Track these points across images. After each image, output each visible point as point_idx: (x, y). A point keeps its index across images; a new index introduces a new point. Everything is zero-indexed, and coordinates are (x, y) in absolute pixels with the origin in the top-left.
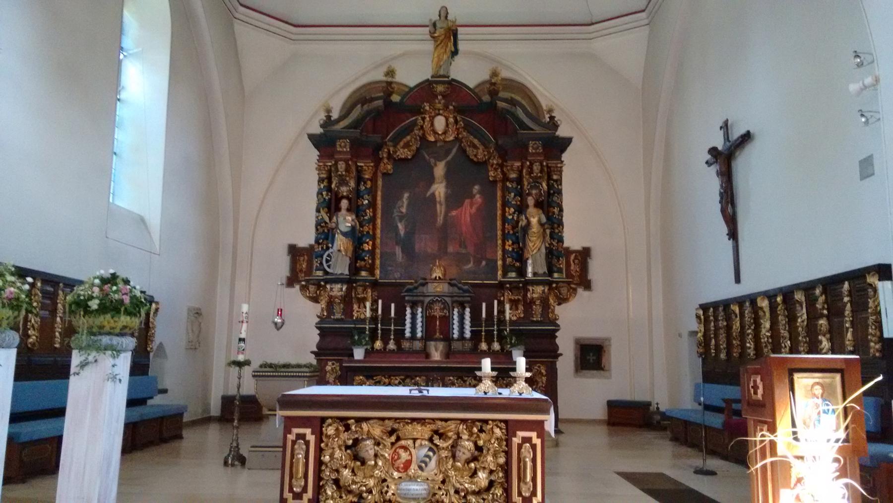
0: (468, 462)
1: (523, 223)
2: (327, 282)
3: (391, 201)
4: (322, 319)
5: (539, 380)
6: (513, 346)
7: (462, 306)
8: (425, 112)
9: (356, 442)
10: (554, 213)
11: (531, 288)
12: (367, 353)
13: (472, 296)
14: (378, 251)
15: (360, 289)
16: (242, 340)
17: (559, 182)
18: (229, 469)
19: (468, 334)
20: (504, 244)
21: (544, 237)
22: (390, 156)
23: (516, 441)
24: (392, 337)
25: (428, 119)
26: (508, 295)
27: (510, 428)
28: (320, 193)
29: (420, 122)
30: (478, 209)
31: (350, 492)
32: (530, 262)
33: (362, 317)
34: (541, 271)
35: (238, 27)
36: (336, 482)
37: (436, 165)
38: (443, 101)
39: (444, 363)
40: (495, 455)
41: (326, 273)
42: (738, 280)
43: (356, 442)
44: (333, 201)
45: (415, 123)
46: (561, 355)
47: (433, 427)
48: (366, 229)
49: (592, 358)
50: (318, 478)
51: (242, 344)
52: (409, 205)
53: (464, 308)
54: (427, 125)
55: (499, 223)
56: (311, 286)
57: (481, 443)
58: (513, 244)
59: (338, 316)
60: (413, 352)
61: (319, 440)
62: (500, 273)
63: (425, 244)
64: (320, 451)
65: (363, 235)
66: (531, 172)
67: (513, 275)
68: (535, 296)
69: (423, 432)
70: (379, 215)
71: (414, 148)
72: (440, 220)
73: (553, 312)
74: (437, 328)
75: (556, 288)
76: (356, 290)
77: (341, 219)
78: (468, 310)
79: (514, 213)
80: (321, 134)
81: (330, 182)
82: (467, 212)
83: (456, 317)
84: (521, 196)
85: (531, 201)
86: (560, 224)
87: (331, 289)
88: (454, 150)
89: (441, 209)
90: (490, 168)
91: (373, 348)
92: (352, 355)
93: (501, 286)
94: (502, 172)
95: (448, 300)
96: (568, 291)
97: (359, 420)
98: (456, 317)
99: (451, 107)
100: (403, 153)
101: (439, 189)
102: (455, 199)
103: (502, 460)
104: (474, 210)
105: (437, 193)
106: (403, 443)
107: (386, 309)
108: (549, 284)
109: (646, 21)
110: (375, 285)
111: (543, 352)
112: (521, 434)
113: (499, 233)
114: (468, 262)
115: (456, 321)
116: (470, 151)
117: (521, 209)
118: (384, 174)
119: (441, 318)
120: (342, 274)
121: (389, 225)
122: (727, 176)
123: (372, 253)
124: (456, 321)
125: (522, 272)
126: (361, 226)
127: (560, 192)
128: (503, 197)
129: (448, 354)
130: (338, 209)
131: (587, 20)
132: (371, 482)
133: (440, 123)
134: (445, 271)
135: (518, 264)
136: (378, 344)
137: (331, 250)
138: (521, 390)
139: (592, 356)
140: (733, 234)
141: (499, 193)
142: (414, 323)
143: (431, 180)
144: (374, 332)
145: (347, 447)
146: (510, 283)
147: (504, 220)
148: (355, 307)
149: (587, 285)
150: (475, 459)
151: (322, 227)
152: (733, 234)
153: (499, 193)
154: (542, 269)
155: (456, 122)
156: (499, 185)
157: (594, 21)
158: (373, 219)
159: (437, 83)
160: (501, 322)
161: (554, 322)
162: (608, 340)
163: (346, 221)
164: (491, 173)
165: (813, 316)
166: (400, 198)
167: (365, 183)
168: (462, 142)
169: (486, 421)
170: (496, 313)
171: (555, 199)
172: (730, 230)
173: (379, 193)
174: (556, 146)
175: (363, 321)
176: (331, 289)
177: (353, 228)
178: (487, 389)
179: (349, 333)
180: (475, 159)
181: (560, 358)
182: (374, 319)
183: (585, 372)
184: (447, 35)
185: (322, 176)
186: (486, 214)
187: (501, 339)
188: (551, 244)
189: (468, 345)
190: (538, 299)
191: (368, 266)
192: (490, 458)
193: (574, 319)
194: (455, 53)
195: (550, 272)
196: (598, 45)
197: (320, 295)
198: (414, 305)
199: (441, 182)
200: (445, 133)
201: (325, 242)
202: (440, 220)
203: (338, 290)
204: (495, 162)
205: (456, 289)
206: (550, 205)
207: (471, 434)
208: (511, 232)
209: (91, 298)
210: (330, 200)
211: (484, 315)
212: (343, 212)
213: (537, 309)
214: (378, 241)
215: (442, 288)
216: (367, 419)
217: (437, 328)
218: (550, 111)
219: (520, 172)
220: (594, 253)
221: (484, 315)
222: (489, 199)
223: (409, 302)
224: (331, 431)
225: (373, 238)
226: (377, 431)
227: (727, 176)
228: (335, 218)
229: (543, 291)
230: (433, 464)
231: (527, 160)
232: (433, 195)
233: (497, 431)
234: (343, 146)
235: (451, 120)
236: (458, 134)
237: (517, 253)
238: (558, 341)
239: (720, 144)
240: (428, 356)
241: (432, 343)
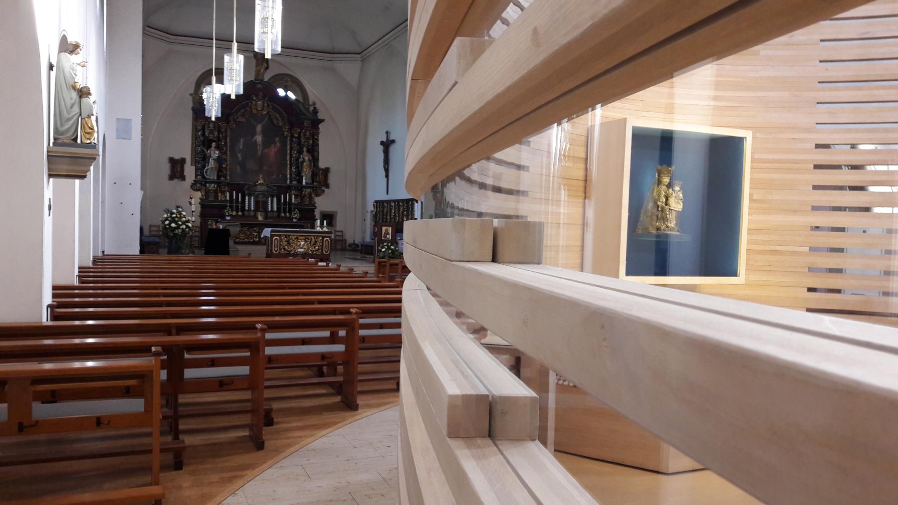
7: (272, 197)
17: (317, 140)
19: (275, 209)
20: (291, 168)
27: (323, 237)
60: (249, 217)
63: (251, 165)
66: (305, 135)
72: (260, 153)
74: (261, 206)
82: (273, 151)
85: (305, 149)
86: (318, 160)
89: (260, 148)
101: (259, 138)
102: (267, 144)
108: (313, 188)
110: (229, 184)
117: (300, 152)
125: (300, 181)
127: (318, 145)
129: (266, 218)
138: (325, 229)
139: (329, 218)
140: (387, 176)
152: (387, 176)
155: (268, 105)
165: (404, 210)
174: (316, 123)
178: (319, 229)
189: (276, 214)
195: (313, 182)
196: (336, 64)
198: (250, 195)
202: (260, 153)
206: (314, 151)
212: (213, 148)
215: (264, 188)
218: (314, 104)
219: (300, 134)
222: (284, 145)
239: (385, 140)
240: (257, 218)
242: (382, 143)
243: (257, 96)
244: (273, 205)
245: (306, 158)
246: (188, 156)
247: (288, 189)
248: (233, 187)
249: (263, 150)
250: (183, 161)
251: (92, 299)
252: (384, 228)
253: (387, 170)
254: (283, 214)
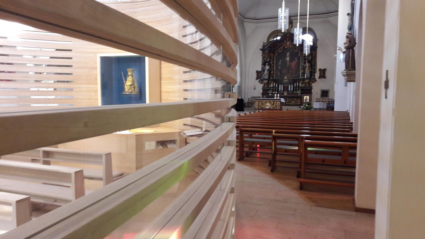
7: (291, 84)
19: (292, 90)
35: (245, 23)
63: (284, 71)
72: (288, 65)
82: (294, 64)
85: (307, 61)
89: (288, 63)
101: (288, 59)
102: (291, 61)
117: (305, 63)
125: (304, 76)
129: (288, 94)
138: (278, 98)
162: (329, 90)
178: (275, 98)
198: (281, 84)
202: (288, 65)
215: (287, 81)
243: (286, 40)
244: (291, 88)
245: (307, 65)
247: (299, 81)
248: (275, 81)
249: (290, 63)
251: (353, 138)
252: (305, 97)
254: (295, 92)
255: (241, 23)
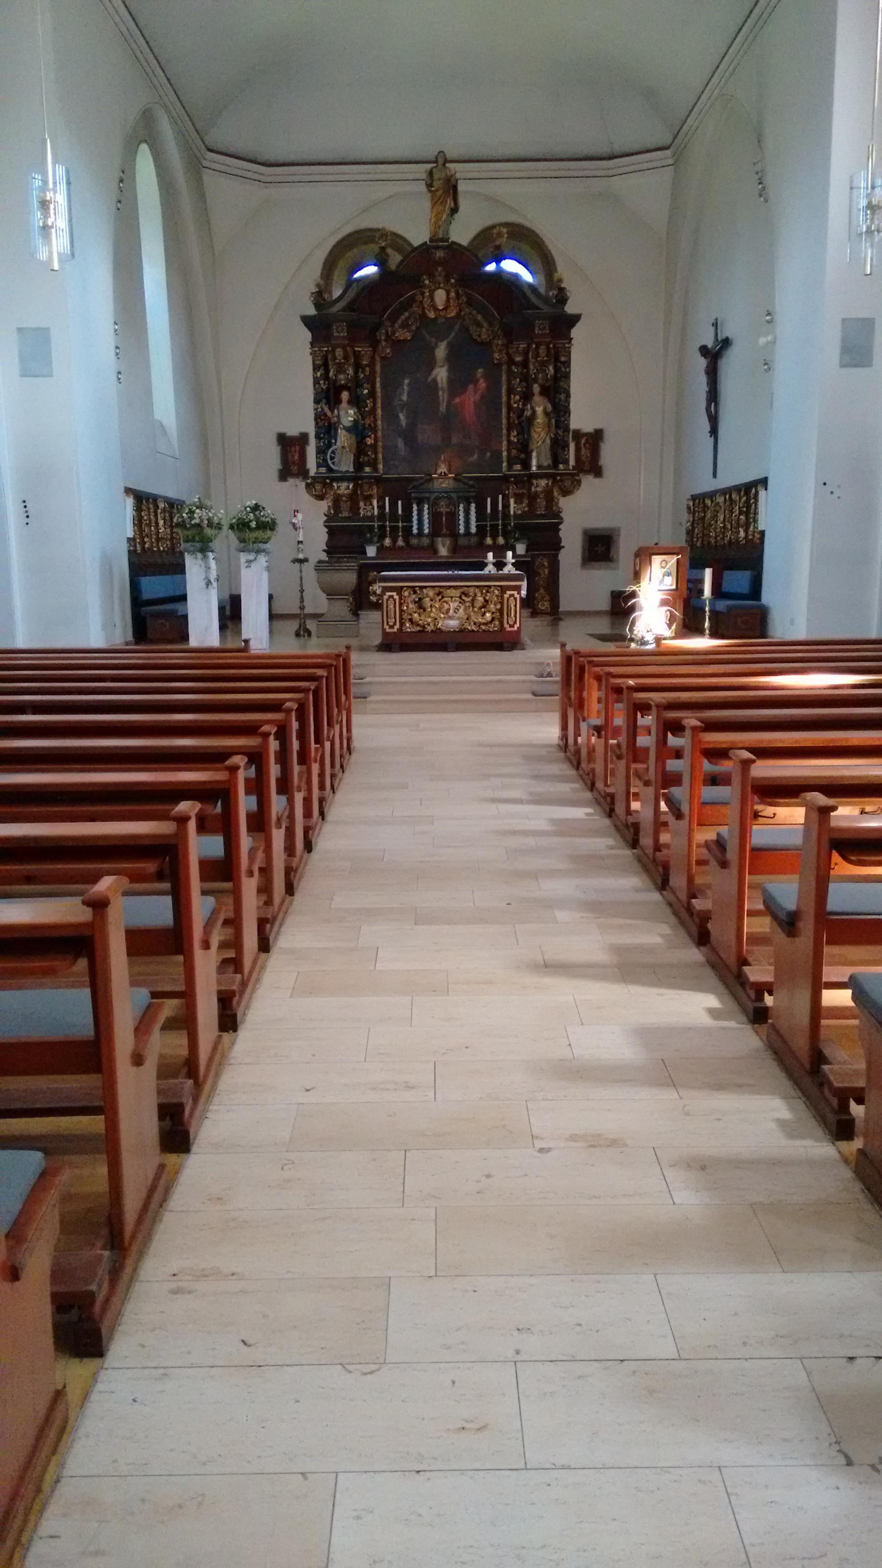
0: (480, 608)
1: (528, 413)
2: (333, 480)
3: (391, 387)
4: (330, 518)
5: (541, 572)
6: (517, 540)
8: (424, 286)
9: (420, 599)
10: (560, 400)
11: (535, 482)
12: (379, 550)
13: (476, 491)
14: (380, 444)
15: (366, 487)
16: (300, 542)
17: (567, 364)
18: (302, 640)
19: (473, 530)
20: (509, 435)
21: (549, 427)
22: (388, 337)
23: (506, 596)
24: (400, 534)
25: (427, 294)
26: (512, 489)
27: (503, 590)
28: (316, 382)
29: (419, 298)
30: (482, 397)
31: (418, 625)
32: (534, 454)
33: (369, 514)
34: (545, 464)
35: (208, 177)
36: (411, 620)
37: (436, 344)
38: (443, 274)
39: (452, 558)
40: (495, 604)
41: (330, 470)
42: (715, 475)
43: (420, 599)
44: (332, 391)
45: (412, 299)
46: (563, 547)
47: (462, 590)
48: (368, 421)
49: (600, 549)
50: (401, 618)
51: (301, 546)
52: (409, 394)
53: (469, 503)
54: (427, 302)
55: (504, 410)
56: (317, 484)
57: (487, 598)
58: (518, 434)
59: (345, 514)
60: (419, 549)
61: (400, 599)
62: (505, 464)
63: (427, 434)
64: (401, 605)
65: (364, 428)
67: (518, 467)
68: (539, 489)
69: (456, 593)
70: (379, 405)
71: (414, 328)
72: (443, 408)
73: (557, 504)
74: (443, 524)
75: (561, 481)
76: (361, 488)
77: (342, 413)
78: (473, 506)
79: (519, 401)
80: (315, 316)
81: (327, 371)
82: (471, 398)
83: (462, 514)
84: (527, 382)
85: (536, 388)
87: (338, 487)
88: (457, 327)
89: (443, 396)
90: (494, 348)
91: (382, 545)
92: (365, 553)
93: (506, 479)
94: (508, 354)
95: (454, 495)
96: (572, 483)
97: (421, 588)
98: (462, 514)
99: (453, 281)
100: (403, 335)
101: (441, 374)
102: (457, 385)
103: (499, 607)
104: (477, 397)
105: (439, 379)
106: (446, 599)
107: (393, 505)
108: (553, 476)
109: (670, 161)
110: (379, 481)
111: (543, 539)
112: (509, 593)
113: (504, 421)
114: (473, 454)
115: (462, 517)
116: (473, 329)
117: (527, 397)
118: (382, 358)
119: (447, 514)
120: (347, 471)
121: (391, 416)
122: (712, 373)
123: (374, 447)
124: (462, 517)
125: (526, 465)
126: (363, 418)
128: (509, 381)
129: (455, 549)
130: (339, 401)
131: (606, 150)
132: (429, 620)
133: (440, 296)
134: (450, 466)
135: (523, 456)
136: (387, 542)
137: (334, 447)
140: (714, 432)
141: (504, 378)
142: (421, 520)
143: (431, 364)
144: (382, 528)
145: (415, 602)
146: (515, 476)
147: (509, 408)
148: (362, 504)
149: (597, 472)
150: (484, 607)
151: (322, 420)
152: (714, 432)
153: (504, 378)
154: (546, 462)
155: (458, 295)
156: (504, 367)
157: (617, 148)
158: (374, 409)
159: (438, 248)
160: (506, 515)
161: (557, 515)
163: (348, 415)
164: (496, 356)
166: (401, 385)
167: (364, 370)
168: (464, 320)
169: (490, 587)
170: (500, 508)
171: (562, 384)
172: (711, 428)
173: (378, 379)
175: (372, 518)
176: (338, 487)
177: (355, 422)
179: (360, 532)
180: (479, 340)
181: (562, 551)
182: (382, 516)
183: (594, 563)
184: (445, 191)
185: (317, 362)
186: (490, 402)
187: (505, 535)
188: (556, 434)
189: (474, 540)
190: (542, 492)
191: (371, 461)
192: (492, 606)
193: (581, 511)
194: (455, 210)
195: (555, 464)
196: (617, 183)
197: (326, 493)
199: (443, 366)
200: (445, 309)
201: (326, 436)
202: (443, 408)
203: (344, 488)
204: (500, 342)
205: (462, 485)
206: (557, 392)
207: (482, 594)
208: (516, 422)
209: (251, 521)
210: (328, 389)
211: (489, 511)
212: (344, 405)
213: (541, 502)
214: (380, 434)
216: (425, 587)
217: (443, 524)
220: (607, 435)
221: (489, 511)
223: (415, 498)
224: (406, 594)
225: (375, 431)
226: (431, 593)
227: (712, 373)
228: (336, 411)
229: (547, 484)
230: (461, 610)
231: (533, 342)
232: (435, 381)
233: (496, 591)
234: (340, 332)
235: (453, 294)
236: (460, 311)
237: (521, 444)
238: (561, 534)
240: (435, 552)
241: (440, 539)
242: (704, 351)
246: (310, 428)
250: (304, 437)
253: (714, 420)
255: (195, 167)
